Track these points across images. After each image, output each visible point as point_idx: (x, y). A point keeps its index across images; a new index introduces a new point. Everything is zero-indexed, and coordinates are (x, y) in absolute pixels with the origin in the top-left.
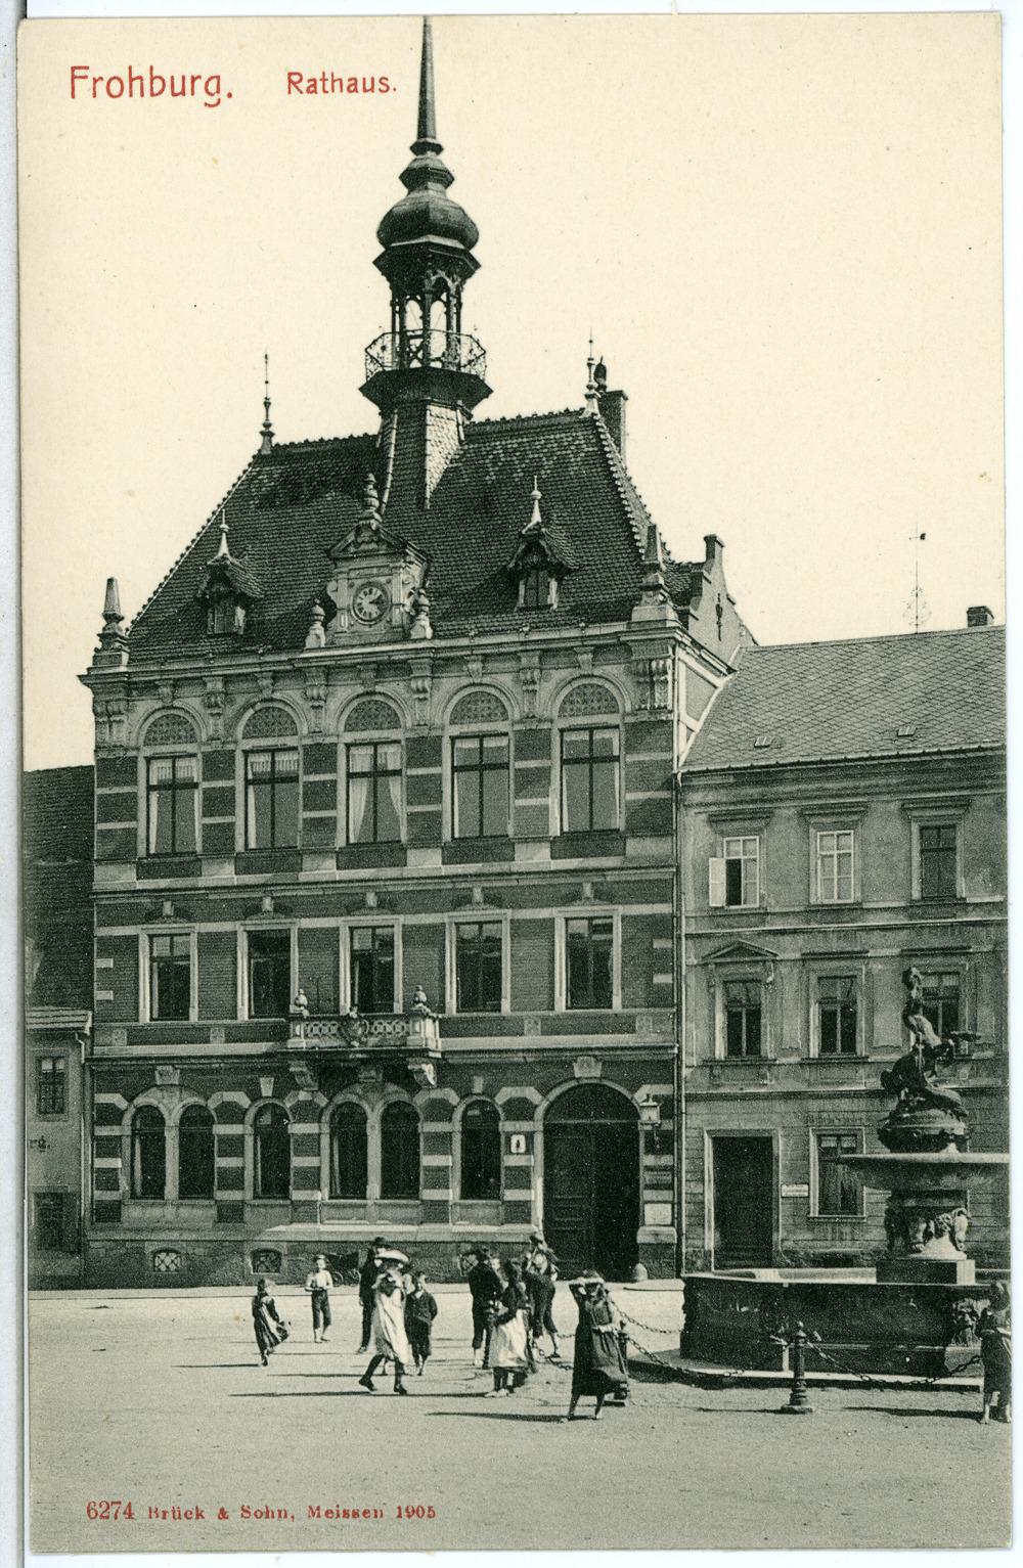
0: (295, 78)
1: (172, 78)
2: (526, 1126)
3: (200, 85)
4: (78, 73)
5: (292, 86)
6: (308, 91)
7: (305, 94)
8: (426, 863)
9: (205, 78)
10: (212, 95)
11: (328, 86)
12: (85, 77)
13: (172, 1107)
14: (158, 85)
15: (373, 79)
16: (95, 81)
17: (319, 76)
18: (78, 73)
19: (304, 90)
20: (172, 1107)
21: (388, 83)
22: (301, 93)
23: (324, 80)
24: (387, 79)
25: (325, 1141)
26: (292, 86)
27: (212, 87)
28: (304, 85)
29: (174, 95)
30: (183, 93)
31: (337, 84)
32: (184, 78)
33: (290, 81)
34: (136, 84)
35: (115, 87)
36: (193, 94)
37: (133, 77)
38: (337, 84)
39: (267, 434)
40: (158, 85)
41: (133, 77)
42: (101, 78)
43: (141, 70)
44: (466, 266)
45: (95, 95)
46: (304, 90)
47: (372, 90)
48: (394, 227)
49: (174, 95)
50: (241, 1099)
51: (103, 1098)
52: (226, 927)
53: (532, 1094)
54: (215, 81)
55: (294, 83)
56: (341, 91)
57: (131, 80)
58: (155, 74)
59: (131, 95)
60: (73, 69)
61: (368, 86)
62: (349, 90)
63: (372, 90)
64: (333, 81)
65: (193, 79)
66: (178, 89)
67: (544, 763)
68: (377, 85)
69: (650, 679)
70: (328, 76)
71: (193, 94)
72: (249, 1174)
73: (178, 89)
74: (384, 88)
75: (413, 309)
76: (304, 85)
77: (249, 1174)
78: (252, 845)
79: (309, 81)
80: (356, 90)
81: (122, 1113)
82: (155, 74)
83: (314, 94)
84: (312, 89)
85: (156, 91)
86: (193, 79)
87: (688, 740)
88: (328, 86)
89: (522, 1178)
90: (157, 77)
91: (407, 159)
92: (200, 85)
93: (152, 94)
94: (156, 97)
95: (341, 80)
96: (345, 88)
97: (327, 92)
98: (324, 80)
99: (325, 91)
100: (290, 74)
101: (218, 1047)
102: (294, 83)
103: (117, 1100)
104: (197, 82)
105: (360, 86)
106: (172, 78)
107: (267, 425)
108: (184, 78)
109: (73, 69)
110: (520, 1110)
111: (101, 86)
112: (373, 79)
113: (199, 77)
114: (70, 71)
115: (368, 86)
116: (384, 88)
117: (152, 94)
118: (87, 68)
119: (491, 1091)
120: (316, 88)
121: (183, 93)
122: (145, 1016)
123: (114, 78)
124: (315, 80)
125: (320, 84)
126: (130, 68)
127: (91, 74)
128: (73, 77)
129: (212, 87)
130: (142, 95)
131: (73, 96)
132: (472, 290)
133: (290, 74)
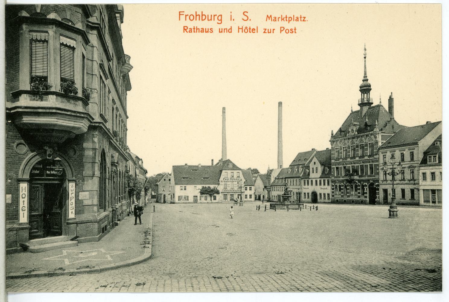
0: (186, 28)
1: (208, 15)
2: (366, 187)
3: (216, 17)
4: (181, 13)
5: (268, 18)
6: (189, 32)
7: (189, 33)
8: (341, 160)
11: (195, 30)
12: (183, 15)
13: (338, 185)
14: (204, 17)
15: (208, 29)
16: (186, 16)
18: (181, 13)
19: (188, 32)
20: (338, 185)
23: (194, 29)
24: (212, 29)
25: (361, 189)
26: (268, 18)
27: (220, 18)
28: (188, 30)
30: (211, 20)
31: (198, 30)
32: (211, 15)
33: (184, 29)
34: (198, 17)
35: (192, 18)
36: (214, 20)
38: (198, 30)
39: (352, 111)
40: (204, 17)
41: (197, 14)
42: (188, 15)
45: (186, 20)
46: (188, 32)
47: (208, 32)
50: (343, 184)
51: (332, 184)
52: (350, 165)
53: (367, 184)
57: (196, 15)
58: (203, 14)
59: (196, 20)
60: (180, 12)
61: (207, 31)
63: (208, 32)
64: (197, 29)
66: (210, 18)
67: (358, 149)
68: (209, 30)
69: (376, 137)
70: (195, 28)
71: (214, 20)
72: (361, 192)
73: (210, 18)
76: (188, 30)
77: (361, 192)
78: (344, 157)
79: (189, 29)
81: (367, 185)
82: (203, 14)
85: (203, 19)
86: (214, 16)
88: (195, 30)
89: (366, 193)
92: (216, 17)
93: (202, 20)
95: (199, 29)
97: (195, 32)
101: (341, 179)
102: (186, 30)
103: (333, 184)
104: (215, 17)
105: (205, 31)
106: (208, 15)
107: (365, 80)
108: (211, 15)
109: (180, 12)
110: (366, 186)
111: (188, 17)
112: (208, 29)
113: (216, 15)
114: (179, 13)
115: (207, 31)
117: (202, 20)
118: (184, 12)
119: (363, 183)
120: (192, 31)
121: (211, 20)
122: (369, 174)
124: (191, 29)
125: (193, 30)
127: (185, 13)
128: (180, 14)
129: (220, 18)
130: (199, 20)
131: (180, 20)
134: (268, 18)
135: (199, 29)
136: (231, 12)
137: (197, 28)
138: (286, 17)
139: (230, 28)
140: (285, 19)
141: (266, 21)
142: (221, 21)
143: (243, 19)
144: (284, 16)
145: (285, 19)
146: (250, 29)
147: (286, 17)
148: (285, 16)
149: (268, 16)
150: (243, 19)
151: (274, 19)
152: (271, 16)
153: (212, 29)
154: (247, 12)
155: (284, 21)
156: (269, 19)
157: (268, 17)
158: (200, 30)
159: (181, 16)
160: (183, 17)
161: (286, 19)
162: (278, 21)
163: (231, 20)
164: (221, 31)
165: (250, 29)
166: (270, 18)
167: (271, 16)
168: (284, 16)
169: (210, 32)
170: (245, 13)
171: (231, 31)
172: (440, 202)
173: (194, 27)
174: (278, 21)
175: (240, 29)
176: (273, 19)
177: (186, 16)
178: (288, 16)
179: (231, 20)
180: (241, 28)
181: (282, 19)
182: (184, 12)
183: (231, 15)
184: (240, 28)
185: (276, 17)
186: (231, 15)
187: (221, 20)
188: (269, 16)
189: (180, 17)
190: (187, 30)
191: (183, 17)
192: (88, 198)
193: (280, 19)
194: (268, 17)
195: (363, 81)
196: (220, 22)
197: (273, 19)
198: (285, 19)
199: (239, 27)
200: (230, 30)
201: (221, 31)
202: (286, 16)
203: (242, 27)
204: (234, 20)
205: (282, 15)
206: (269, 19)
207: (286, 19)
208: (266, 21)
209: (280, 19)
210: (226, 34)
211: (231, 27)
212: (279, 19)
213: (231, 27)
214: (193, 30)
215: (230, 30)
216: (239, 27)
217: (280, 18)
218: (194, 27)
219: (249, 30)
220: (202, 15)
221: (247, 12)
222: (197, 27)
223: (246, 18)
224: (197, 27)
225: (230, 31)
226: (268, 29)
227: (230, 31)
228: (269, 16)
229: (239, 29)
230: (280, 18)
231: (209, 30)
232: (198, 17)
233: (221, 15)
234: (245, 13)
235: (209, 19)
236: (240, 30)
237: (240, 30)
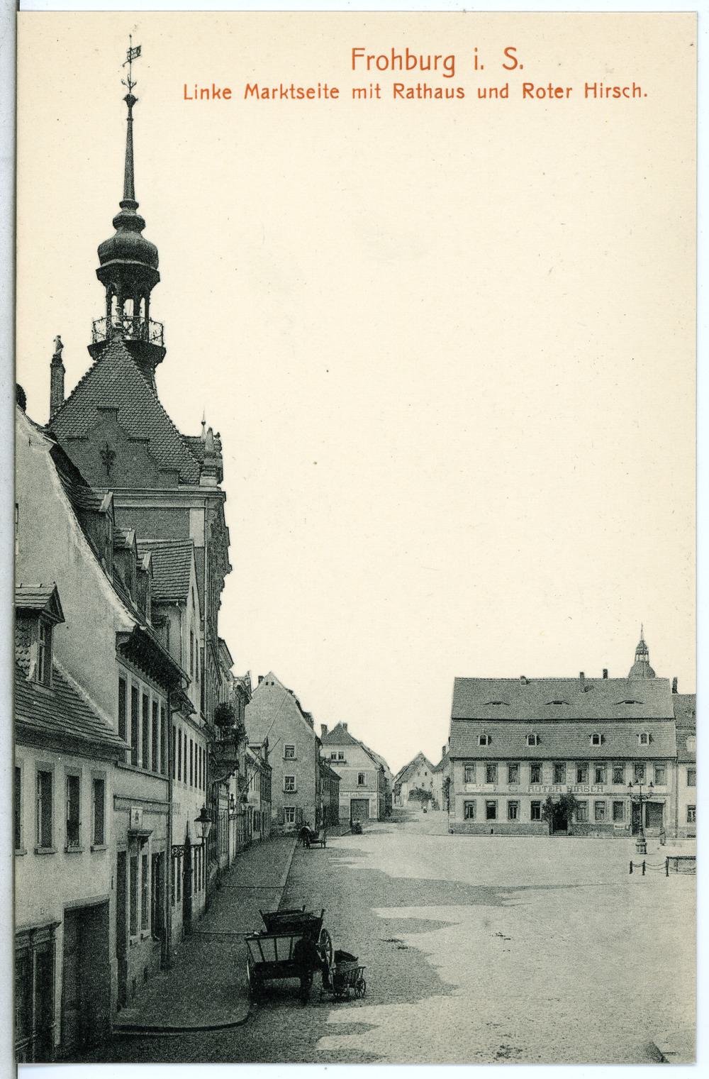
0: (399, 88)
3: (440, 62)
4: (357, 52)
5: (249, 91)
9: (444, 58)
10: (448, 69)
11: (422, 92)
12: (362, 55)
14: (411, 62)
15: (453, 90)
16: (369, 58)
17: (415, 87)
19: (405, 96)
21: (463, 92)
22: (403, 97)
23: (419, 89)
24: (462, 89)
27: (449, 64)
28: (404, 93)
29: (422, 69)
30: (429, 68)
31: (428, 92)
33: (395, 90)
34: (397, 61)
35: (382, 63)
36: (436, 68)
37: (395, 56)
38: (428, 92)
40: (411, 62)
41: (395, 56)
42: (373, 57)
43: (400, 51)
44: (154, 278)
45: (369, 68)
46: (405, 96)
48: (106, 252)
49: (422, 69)
54: (451, 59)
55: (399, 91)
56: (431, 97)
57: (394, 58)
58: (409, 54)
59: (393, 68)
60: (354, 49)
61: (450, 94)
62: (436, 97)
63: (452, 96)
64: (425, 90)
65: (436, 58)
66: (425, 65)
68: (456, 93)
70: (422, 87)
73: (425, 65)
74: (461, 95)
75: (129, 304)
76: (404, 93)
79: (408, 90)
80: (268, 97)
82: (409, 54)
83: (266, 99)
84: (410, 95)
85: (410, 65)
86: (436, 58)
87: (439, 925)
88: (422, 92)
90: (411, 56)
91: (117, 211)
92: (440, 62)
93: (408, 68)
94: (411, 70)
95: (430, 90)
96: (433, 95)
98: (419, 89)
99: (419, 97)
100: (395, 85)
106: (421, 57)
109: (354, 49)
111: (373, 62)
112: (453, 90)
113: (373, 57)
115: (450, 94)
116: (461, 95)
117: (408, 68)
118: (363, 49)
121: (429, 68)
123: (382, 56)
124: (412, 89)
125: (416, 92)
126: (393, 50)
127: (367, 53)
128: (354, 56)
129: (449, 64)
130: (401, 68)
131: (354, 68)
132: (156, 293)
133: (395, 85)
134: (249, 92)
135: (430, 90)
136: (476, 50)
137: (427, 88)
138: (292, 89)
139: (505, 87)
140: (289, 93)
141: (246, 97)
142: (453, 72)
143: (504, 66)
144: (287, 86)
145: (289, 93)
146: (550, 89)
147: (292, 89)
148: (290, 88)
149: (248, 87)
150: (504, 66)
151: (263, 94)
152: (256, 87)
153: (461, 91)
154: (514, 49)
155: (219, 97)
156: (252, 95)
157: (250, 90)
158: (434, 93)
159: (356, 58)
160: (360, 62)
161: (292, 94)
162: (274, 97)
163: (476, 68)
164: (482, 94)
165: (550, 89)
166: (255, 91)
167: (256, 87)
168: (287, 86)
169: (458, 96)
170: (510, 52)
171: (507, 94)
172: (694, 820)
173: (419, 85)
174: (274, 97)
175: (592, 89)
176: (261, 92)
177: (369, 58)
178: (296, 87)
179: (476, 68)
180: (593, 86)
181: (282, 95)
182: (363, 49)
183: (476, 57)
184: (589, 86)
185: (267, 89)
186: (476, 57)
187: (452, 68)
188: (252, 87)
189: (354, 60)
190: (402, 93)
191: (360, 62)
192: (591, 763)
193: (278, 94)
194: (250, 90)
195: (122, 205)
196: (449, 73)
197: (261, 92)
198: (289, 93)
199: (586, 84)
200: (504, 93)
201: (482, 94)
202: (292, 85)
203: (595, 84)
204: (482, 68)
205: (281, 85)
206: (252, 95)
207: (292, 94)
208: (246, 97)
209: (278, 94)
210: (494, 102)
211: (507, 84)
212: (276, 92)
213: (507, 84)
214: (416, 92)
215: (504, 93)
216: (586, 84)
217: (277, 90)
218: (419, 85)
219: (547, 92)
220: (408, 57)
221: (514, 49)
222: (425, 85)
223: (511, 63)
224: (425, 85)
225: (504, 93)
226: (640, 96)
227: (504, 93)
228: (252, 87)
229: (587, 88)
230: (277, 90)
231: (456, 93)
232: (397, 61)
233: (453, 57)
234: (510, 52)
235: (424, 67)
236: (591, 92)
237: (591, 92)
